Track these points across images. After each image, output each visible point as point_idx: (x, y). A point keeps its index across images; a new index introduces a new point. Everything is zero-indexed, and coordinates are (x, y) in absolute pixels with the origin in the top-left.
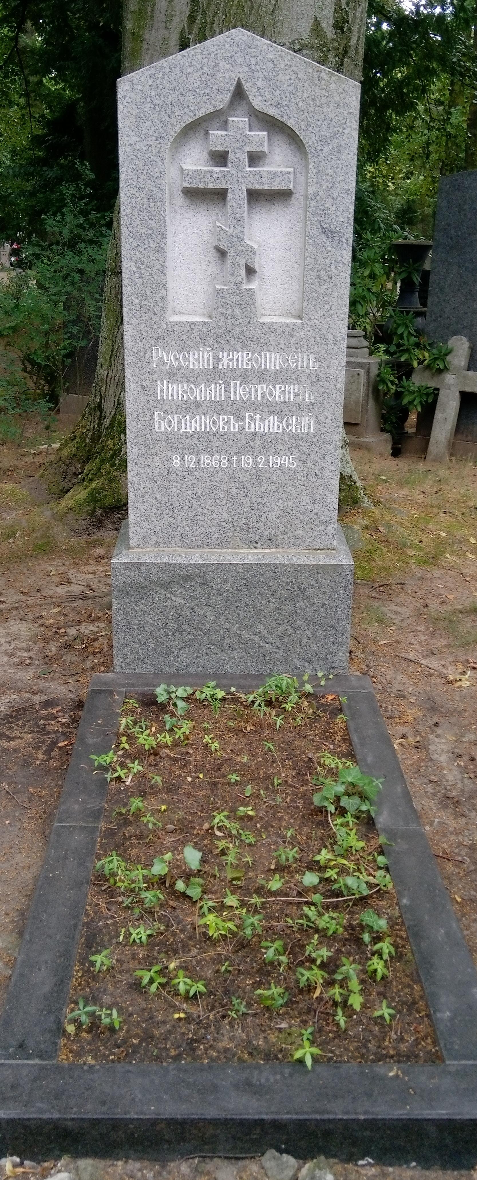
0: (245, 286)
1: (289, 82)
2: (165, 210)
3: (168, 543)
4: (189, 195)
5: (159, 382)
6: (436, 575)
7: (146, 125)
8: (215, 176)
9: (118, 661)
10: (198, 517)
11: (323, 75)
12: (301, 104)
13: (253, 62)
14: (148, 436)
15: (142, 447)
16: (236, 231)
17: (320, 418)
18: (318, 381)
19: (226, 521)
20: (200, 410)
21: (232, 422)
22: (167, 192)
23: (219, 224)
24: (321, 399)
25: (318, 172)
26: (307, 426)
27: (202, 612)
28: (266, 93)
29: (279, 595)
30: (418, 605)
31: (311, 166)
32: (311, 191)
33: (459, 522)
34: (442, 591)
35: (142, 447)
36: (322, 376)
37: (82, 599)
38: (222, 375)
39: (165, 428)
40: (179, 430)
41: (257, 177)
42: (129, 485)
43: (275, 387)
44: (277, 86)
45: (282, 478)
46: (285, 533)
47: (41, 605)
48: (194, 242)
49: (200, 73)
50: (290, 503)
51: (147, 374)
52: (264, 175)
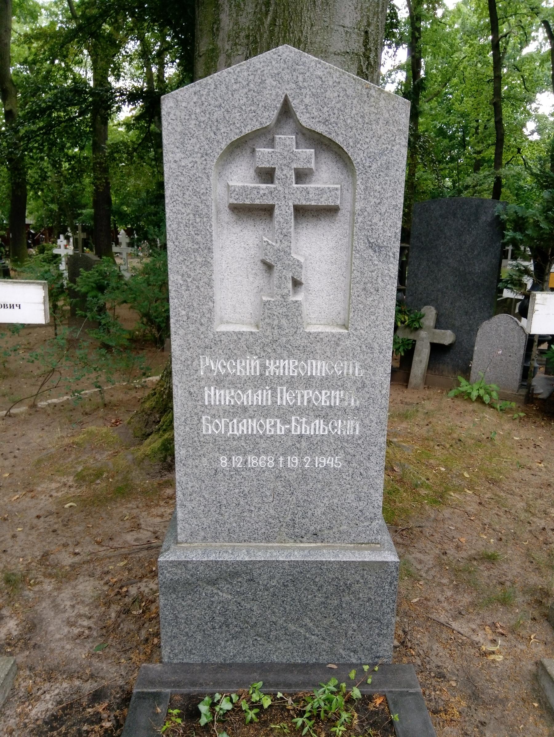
0: (292, 298)
1: (337, 99)
2: (211, 226)
3: (215, 538)
4: (236, 211)
5: (206, 388)
6: (447, 516)
7: (191, 142)
8: (262, 192)
9: (165, 652)
10: (245, 514)
11: (372, 92)
12: (349, 121)
13: (300, 78)
14: (196, 439)
15: (190, 449)
16: (283, 246)
17: (365, 421)
18: (364, 387)
19: (273, 518)
20: (247, 414)
21: (279, 425)
22: (213, 208)
23: (265, 239)
24: (366, 404)
25: (366, 189)
26: (352, 429)
27: (248, 606)
28: (314, 110)
29: (325, 590)
30: (437, 552)
31: (359, 183)
32: (358, 207)
33: (450, 454)
34: (454, 533)
35: (190, 449)
36: (367, 382)
37: (147, 549)
38: (269, 382)
39: (213, 431)
40: (226, 432)
41: (304, 193)
42: (177, 484)
43: (321, 393)
44: (325, 103)
45: (328, 477)
46: (330, 528)
47: (110, 558)
48: (241, 256)
49: (246, 90)
50: (336, 501)
51: (195, 381)
52: (311, 191)
